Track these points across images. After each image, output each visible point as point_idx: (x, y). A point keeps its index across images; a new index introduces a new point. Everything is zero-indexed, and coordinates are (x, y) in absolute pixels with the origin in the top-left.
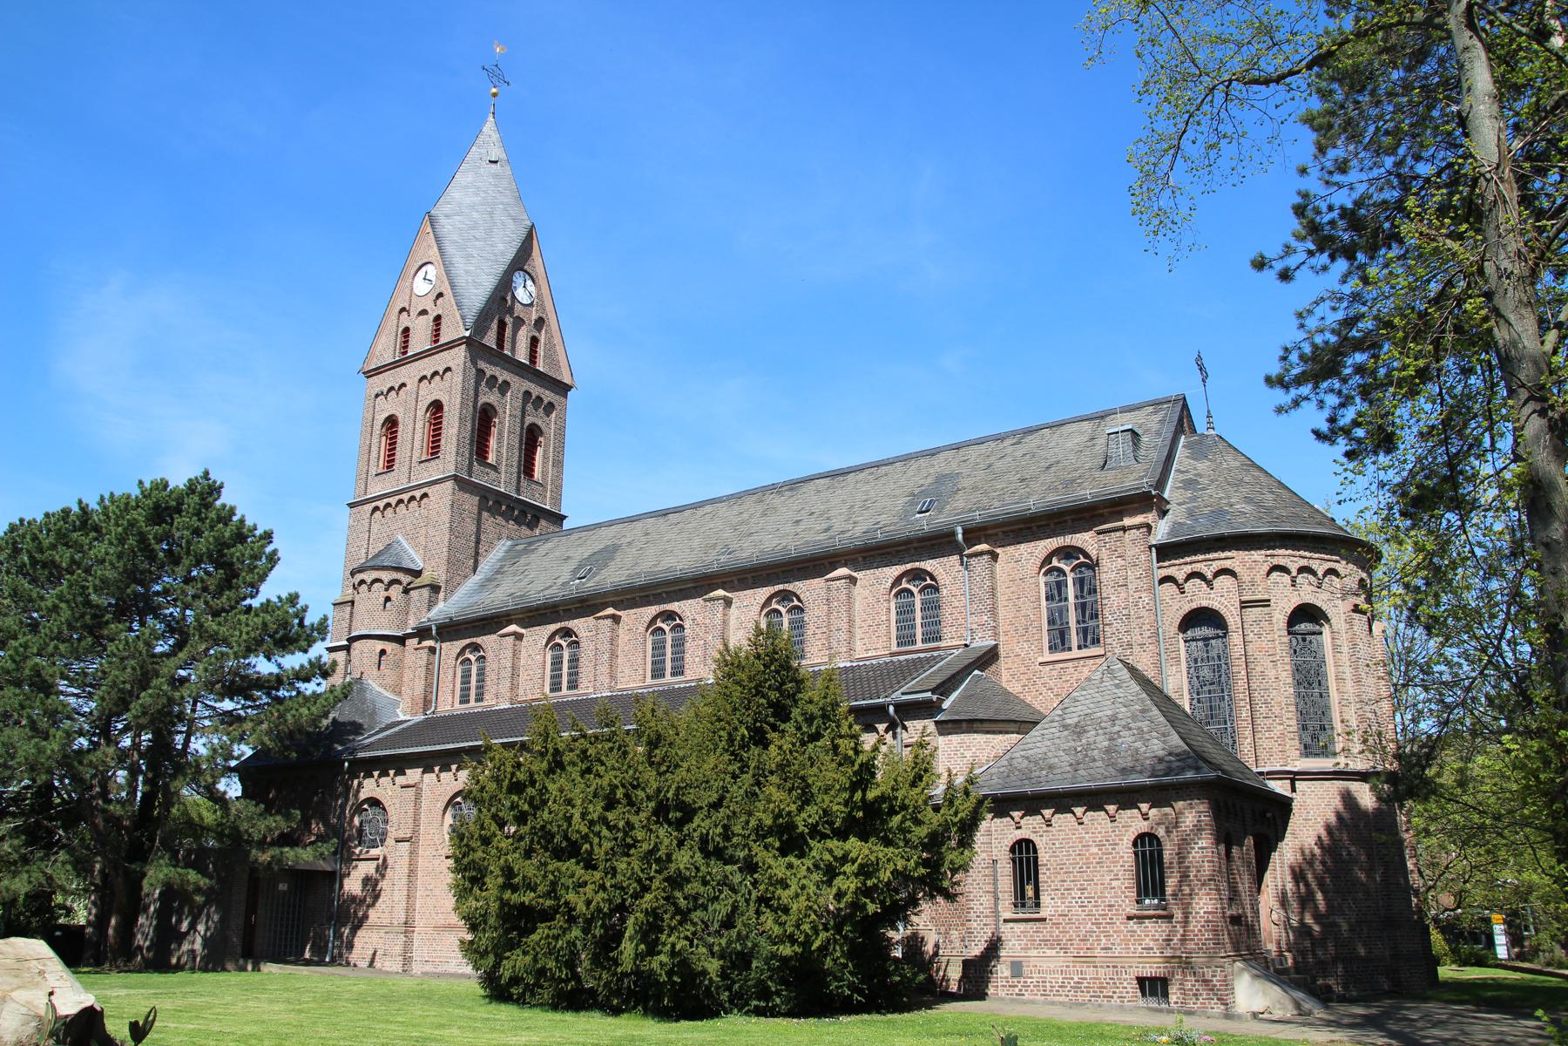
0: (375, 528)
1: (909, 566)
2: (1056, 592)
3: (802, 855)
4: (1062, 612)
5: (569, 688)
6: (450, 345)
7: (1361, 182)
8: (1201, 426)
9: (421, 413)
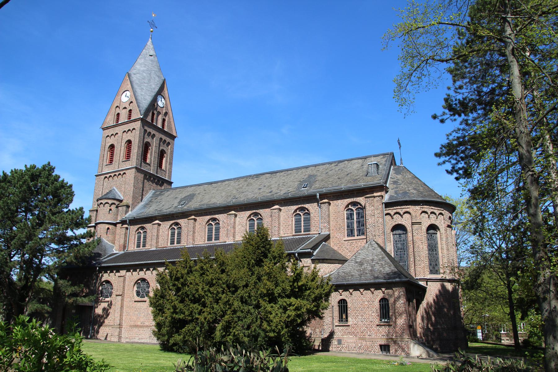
0: (105, 184)
1: (300, 206)
2: (350, 217)
3: (275, 303)
4: (352, 223)
5: (177, 243)
6: (135, 121)
7: (467, 92)
8: (398, 163)
9: (123, 144)
